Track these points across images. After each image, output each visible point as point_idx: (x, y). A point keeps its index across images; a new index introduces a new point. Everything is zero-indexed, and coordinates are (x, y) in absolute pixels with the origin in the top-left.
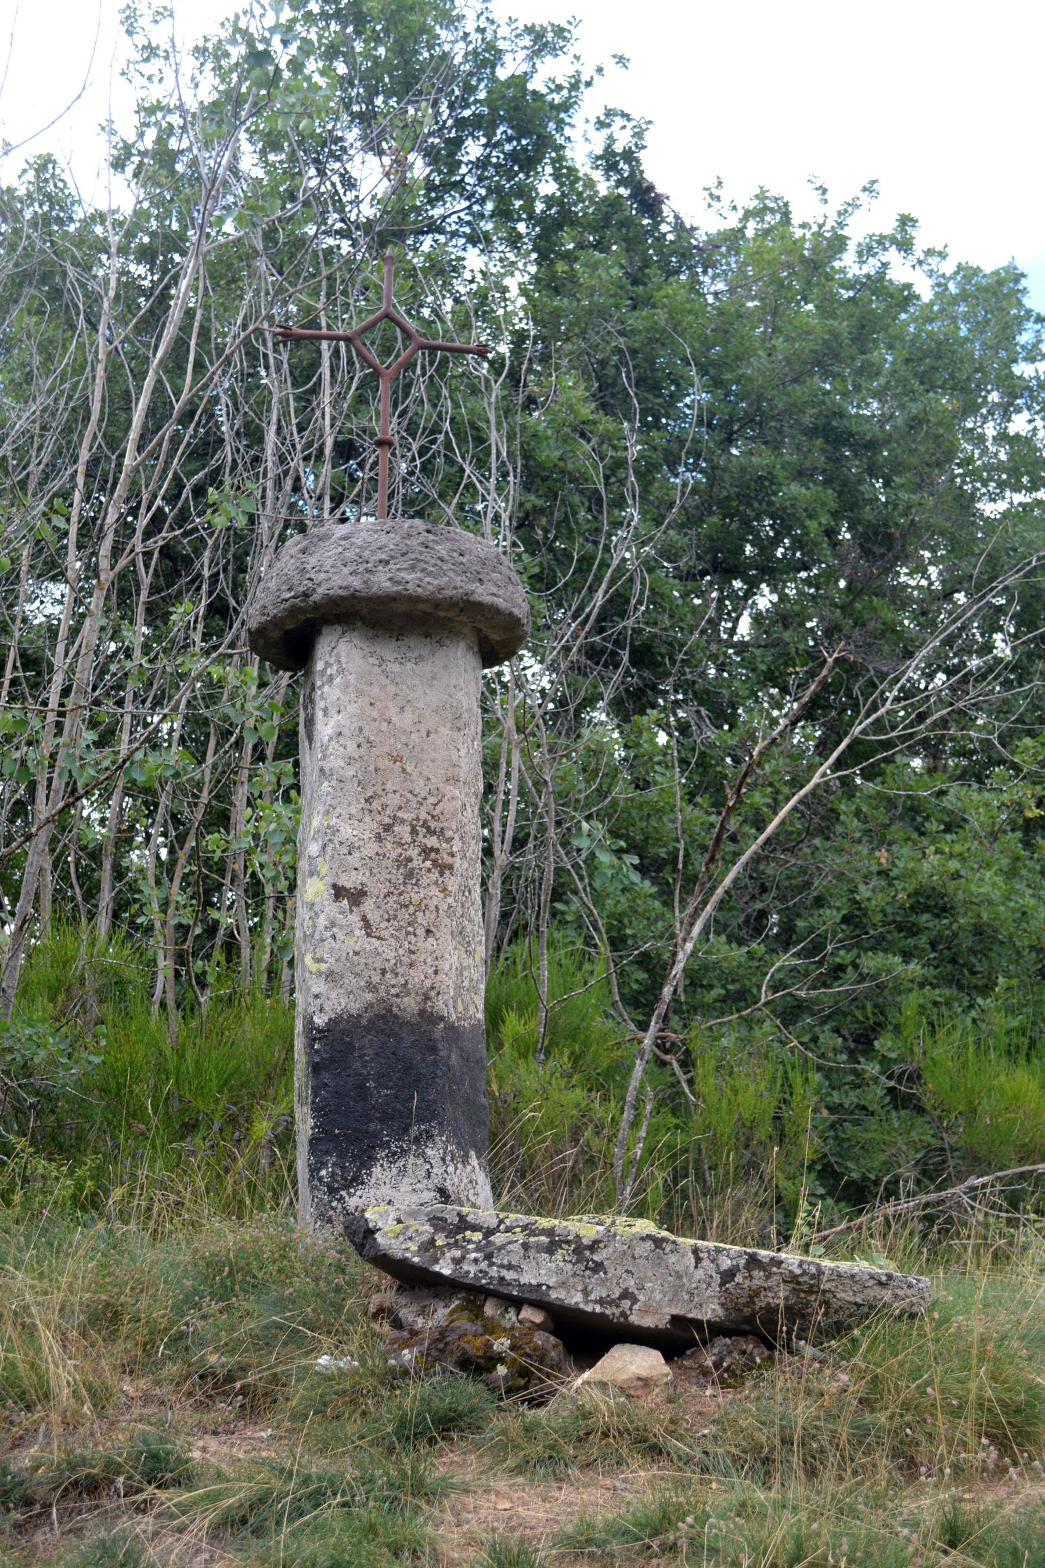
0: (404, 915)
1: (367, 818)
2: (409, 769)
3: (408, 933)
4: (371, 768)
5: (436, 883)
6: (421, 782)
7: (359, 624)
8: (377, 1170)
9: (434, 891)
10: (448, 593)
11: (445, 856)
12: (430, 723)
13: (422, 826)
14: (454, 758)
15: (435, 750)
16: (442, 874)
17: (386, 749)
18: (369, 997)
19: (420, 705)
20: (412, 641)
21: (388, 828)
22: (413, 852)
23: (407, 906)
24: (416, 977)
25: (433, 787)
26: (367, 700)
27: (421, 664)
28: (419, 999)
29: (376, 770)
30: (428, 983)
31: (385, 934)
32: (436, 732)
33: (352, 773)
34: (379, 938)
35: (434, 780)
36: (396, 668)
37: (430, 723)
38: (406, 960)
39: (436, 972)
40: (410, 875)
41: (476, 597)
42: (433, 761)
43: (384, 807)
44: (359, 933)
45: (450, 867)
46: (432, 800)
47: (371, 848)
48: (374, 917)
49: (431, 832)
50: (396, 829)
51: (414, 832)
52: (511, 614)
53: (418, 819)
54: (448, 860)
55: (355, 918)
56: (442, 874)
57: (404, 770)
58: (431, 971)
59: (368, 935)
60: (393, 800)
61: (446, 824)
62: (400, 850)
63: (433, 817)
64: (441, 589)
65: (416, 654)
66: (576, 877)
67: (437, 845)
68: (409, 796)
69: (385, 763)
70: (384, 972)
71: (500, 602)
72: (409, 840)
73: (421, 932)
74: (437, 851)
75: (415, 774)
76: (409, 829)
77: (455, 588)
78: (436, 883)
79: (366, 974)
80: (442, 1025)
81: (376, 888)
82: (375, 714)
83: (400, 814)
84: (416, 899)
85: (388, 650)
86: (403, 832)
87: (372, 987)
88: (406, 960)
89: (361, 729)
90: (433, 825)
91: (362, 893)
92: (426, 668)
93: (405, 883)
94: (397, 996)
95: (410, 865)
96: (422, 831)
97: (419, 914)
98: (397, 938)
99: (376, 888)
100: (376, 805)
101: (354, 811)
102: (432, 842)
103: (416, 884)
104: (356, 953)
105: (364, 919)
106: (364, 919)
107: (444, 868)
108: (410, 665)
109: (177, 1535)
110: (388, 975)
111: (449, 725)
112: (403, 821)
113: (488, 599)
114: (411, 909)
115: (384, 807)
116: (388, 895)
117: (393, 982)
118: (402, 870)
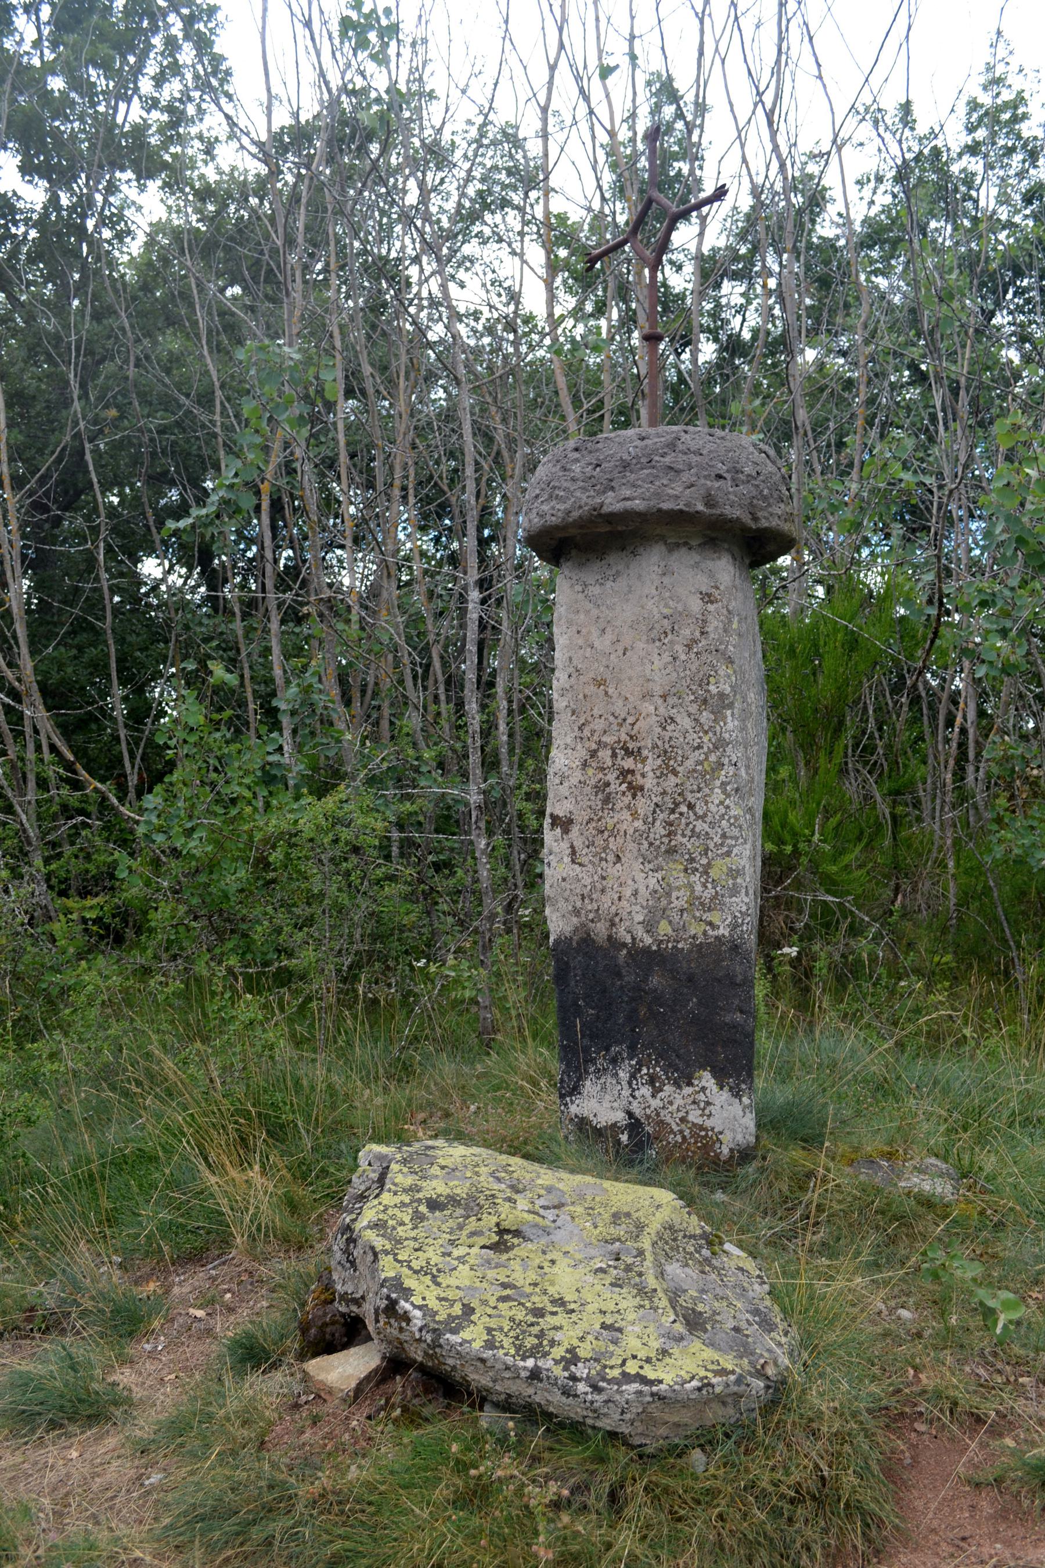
0: (599, 841)
1: (579, 746)
2: (610, 691)
3: (601, 859)
4: (581, 696)
5: (628, 807)
6: (620, 703)
7: (574, 552)
8: (588, 1083)
9: (626, 815)
10: (575, 514)
11: (639, 777)
12: (626, 641)
13: (622, 748)
14: (648, 672)
15: (631, 667)
16: (634, 796)
17: (592, 675)
18: (575, 920)
19: (618, 623)
20: (611, 559)
21: (593, 754)
22: (611, 777)
23: (602, 832)
24: (605, 902)
25: (631, 706)
26: (574, 629)
27: (619, 579)
28: (608, 924)
29: (585, 697)
30: (613, 909)
31: (585, 860)
32: (632, 648)
33: (565, 704)
34: (580, 865)
35: (631, 699)
36: (596, 590)
37: (626, 641)
38: (599, 886)
39: (620, 898)
40: (607, 800)
41: (606, 510)
42: (630, 679)
43: (593, 732)
44: (567, 860)
45: (642, 789)
46: (630, 720)
47: (576, 776)
48: (578, 844)
49: (629, 753)
50: (600, 754)
51: (614, 755)
52: (660, 510)
53: (619, 741)
54: (640, 781)
55: (565, 845)
56: (634, 796)
57: (606, 693)
58: (616, 897)
59: (573, 862)
60: (599, 725)
61: (642, 744)
62: (601, 775)
63: (631, 737)
64: (568, 513)
65: (614, 571)
66: (971, 736)
67: (632, 767)
68: (611, 718)
69: (591, 689)
70: (583, 898)
71: (638, 505)
72: (610, 764)
73: (611, 858)
74: (632, 772)
75: (615, 696)
76: (609, 752)
77: (580, 507)
78: (628, 807)
79: (572, 899)
80: (625, 952)
81: (581, 816)
82: (580, 642)
83: (604, 739)
84: (610, 823)
85: (590, 576)
86: (605, 755)
87: (576, 912)
88: (599, 886)
89: (570, 659)
90: (631, 745)
91: (570, 821)
92: (622, 583)
93: (603, 809)
94: (592, 921)
95: (608, 790)
96: (621, 753)
97: (611, 839)
98: (593, 864)
99: (581, 816)
100: (587, 732)
101: (569, 740)
102: (628, 763)
103: (612, 809)
104: (564, 880)
105: (572, 847)
106: (572, 847)
107: (635, 790)
108: (609, 584)
109: (680, 1328)
110: (587, 901)
111: (644, 638)
112: (606, 745)
113: (618, 507)
114: (606, 833)
115: (593, 732)
116: (590, 820)
117: (589, 907)
118: (600, 796)
